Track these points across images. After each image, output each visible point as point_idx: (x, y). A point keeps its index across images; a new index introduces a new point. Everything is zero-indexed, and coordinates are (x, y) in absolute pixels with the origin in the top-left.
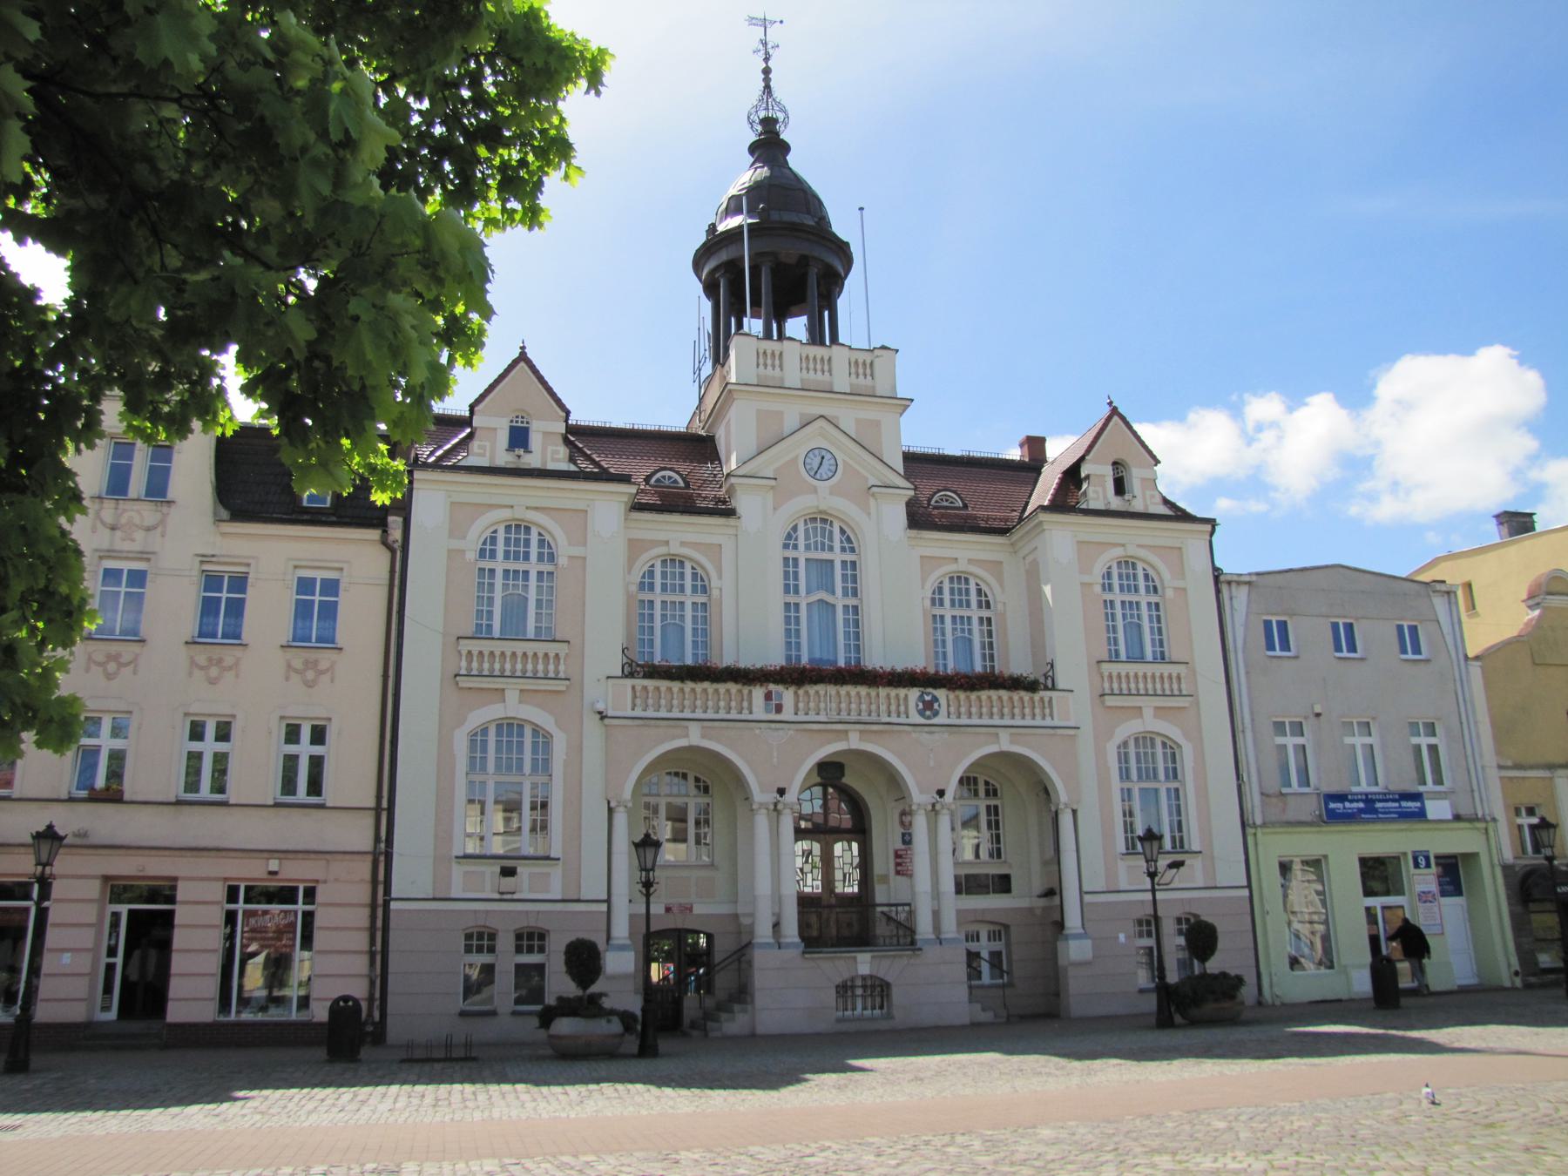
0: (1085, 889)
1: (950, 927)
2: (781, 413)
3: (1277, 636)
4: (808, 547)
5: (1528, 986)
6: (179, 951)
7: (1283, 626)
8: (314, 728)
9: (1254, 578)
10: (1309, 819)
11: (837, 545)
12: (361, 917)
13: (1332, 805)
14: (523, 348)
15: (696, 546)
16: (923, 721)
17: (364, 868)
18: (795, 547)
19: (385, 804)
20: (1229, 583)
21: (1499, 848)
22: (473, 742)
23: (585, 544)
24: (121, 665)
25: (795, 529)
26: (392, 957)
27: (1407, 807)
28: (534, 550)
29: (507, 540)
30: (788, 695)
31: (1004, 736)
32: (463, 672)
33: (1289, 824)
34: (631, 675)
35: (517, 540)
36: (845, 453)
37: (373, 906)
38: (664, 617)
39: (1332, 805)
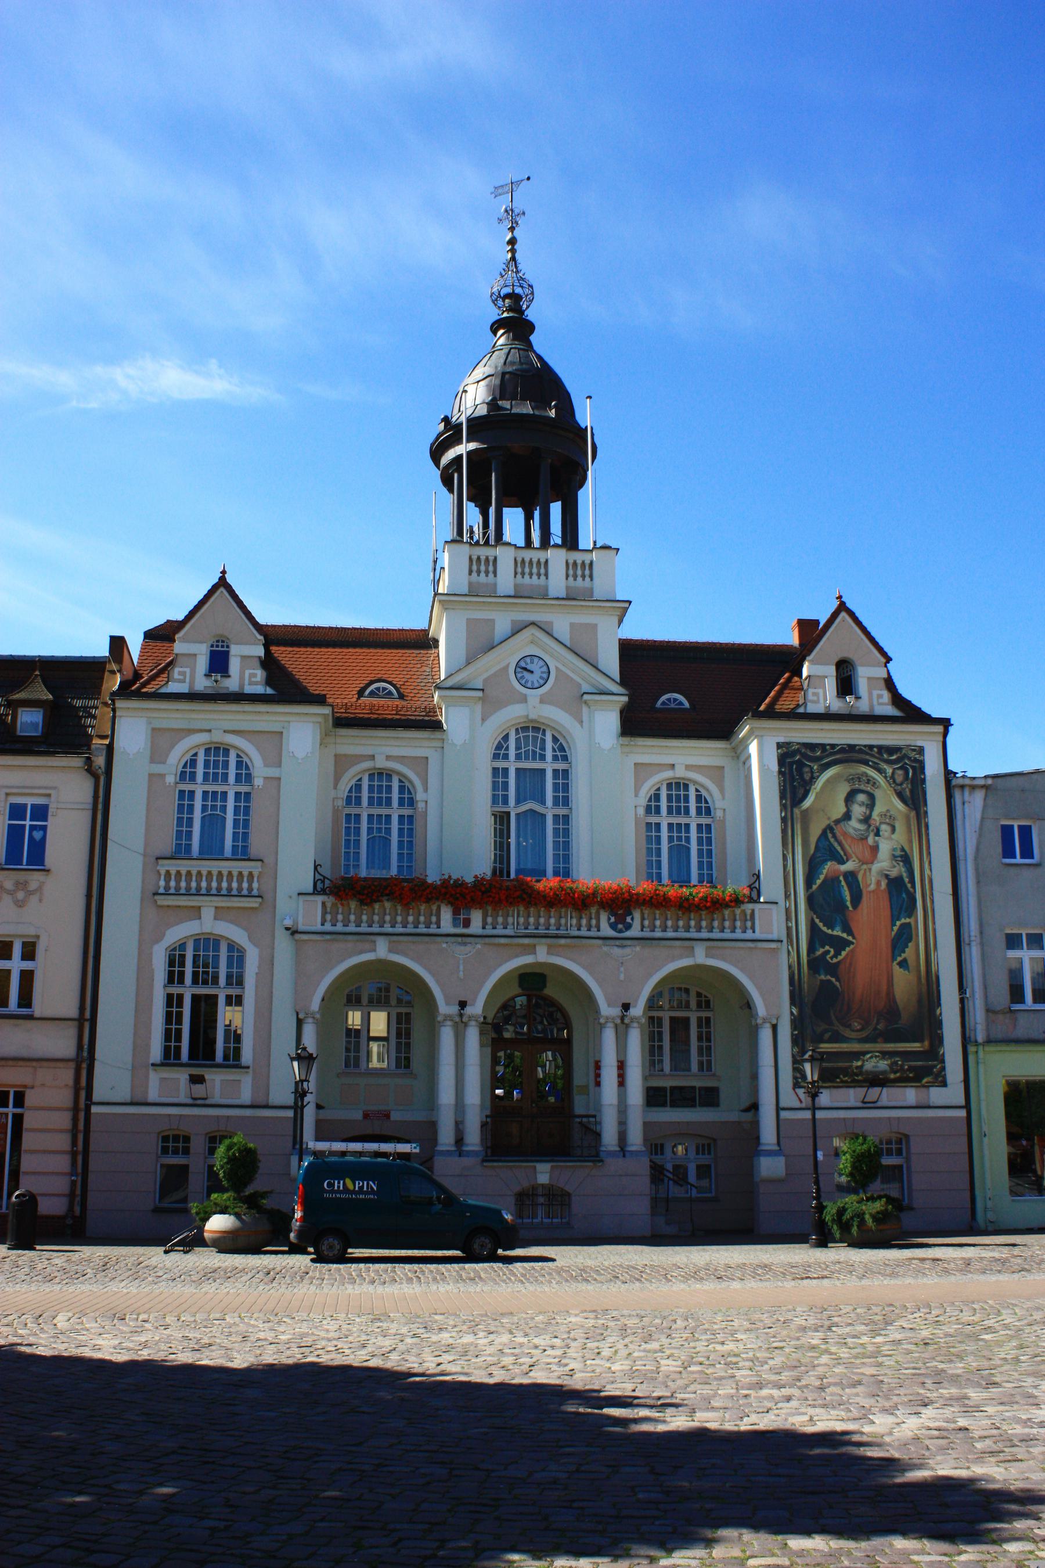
0: (782, 1104)
1: (636, 1138)
2: (493, 621)
3: (1016, 843)
4: (518, 757)
6: (28, 1130)
7: (1026, 832)
8: (25, 945)
9: (990, 781)
12: (64, 1120)
14: (224, 572)
15: (401, 759)
16: (611, 933)
17: (67, 1075)
18: (506, 757)
19: (88, 1015)
20: (962, 787)
23: (279, 765)
24: (31, 893)
25: (506, 738)
26: (92, 1157)
29: (207, 764)
32: (161, 890)
36: (559, 660)
37: (75, 1109)
38: (370, 830)
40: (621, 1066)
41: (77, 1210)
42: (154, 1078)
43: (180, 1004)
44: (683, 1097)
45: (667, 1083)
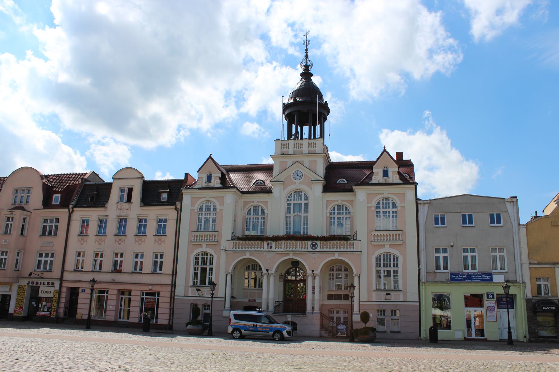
1: (317, 309)
3: (440, 221)
4: (294, 200)
5: (530, 341)
10: (445, 280)
11: (303, 199)
13: (453, 276)
16: (312, 250)
17: (169, 288)
18: (291, 200)
21: (523, 293)
22: (377, 259)
25: (291, 194)
27: (487, 278)
28: (391, 205)
29: (383, 203)
30: (273, 244)
31: (337, 254)
33: (436, 282)
34: (234, 240)
35: (386, 203)
36: (305, 171)
37: (171, 297)
39: (453, 276)
40: (314, 288)
41: (171, 323)
42: (190, 290)
43: (198, 270)
44: (338, 297)
45: (334, 293)
